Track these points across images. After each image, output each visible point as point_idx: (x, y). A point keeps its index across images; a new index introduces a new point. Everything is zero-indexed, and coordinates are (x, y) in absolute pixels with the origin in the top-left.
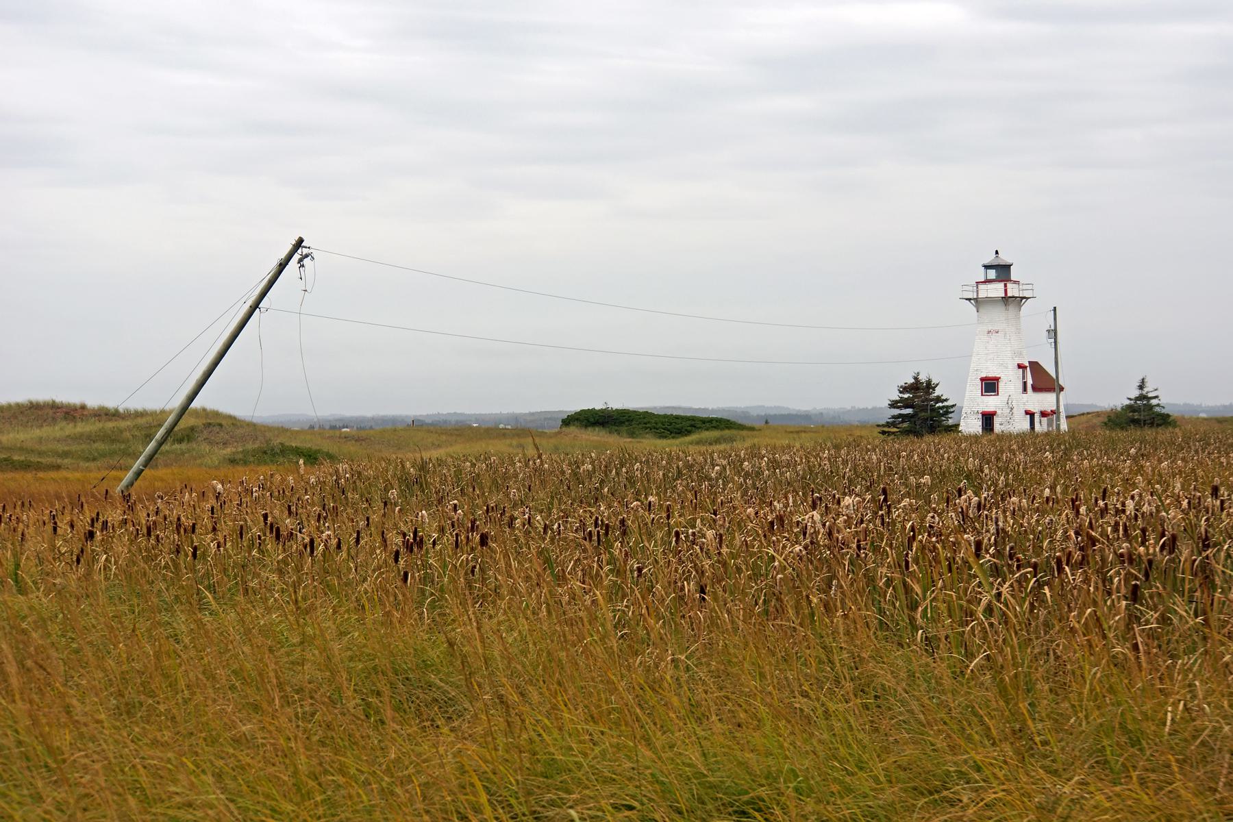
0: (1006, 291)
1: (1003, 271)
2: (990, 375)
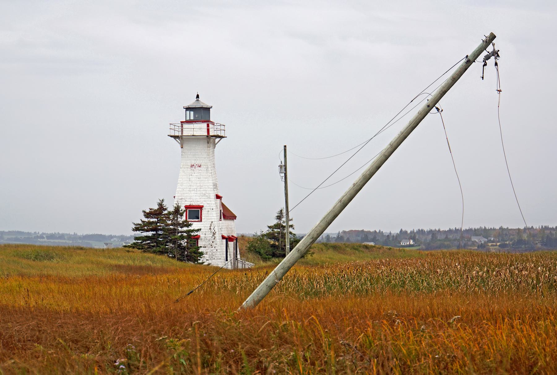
0: (208, 130)
1: (201, 113)
2: (194, 204)
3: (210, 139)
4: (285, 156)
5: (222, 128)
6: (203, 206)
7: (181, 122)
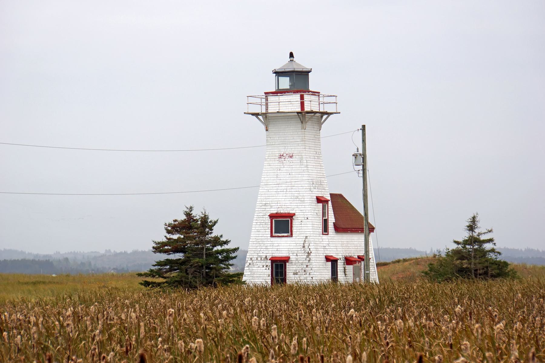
0: (302, 104)
1: (298, 79)
2: (282, 211)
3: (304, 116)
4: (364, 141)
5: (333, 100)
6: (294, 214)
7: (266, 93)
